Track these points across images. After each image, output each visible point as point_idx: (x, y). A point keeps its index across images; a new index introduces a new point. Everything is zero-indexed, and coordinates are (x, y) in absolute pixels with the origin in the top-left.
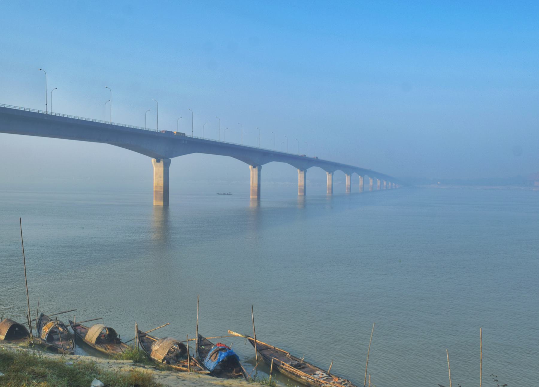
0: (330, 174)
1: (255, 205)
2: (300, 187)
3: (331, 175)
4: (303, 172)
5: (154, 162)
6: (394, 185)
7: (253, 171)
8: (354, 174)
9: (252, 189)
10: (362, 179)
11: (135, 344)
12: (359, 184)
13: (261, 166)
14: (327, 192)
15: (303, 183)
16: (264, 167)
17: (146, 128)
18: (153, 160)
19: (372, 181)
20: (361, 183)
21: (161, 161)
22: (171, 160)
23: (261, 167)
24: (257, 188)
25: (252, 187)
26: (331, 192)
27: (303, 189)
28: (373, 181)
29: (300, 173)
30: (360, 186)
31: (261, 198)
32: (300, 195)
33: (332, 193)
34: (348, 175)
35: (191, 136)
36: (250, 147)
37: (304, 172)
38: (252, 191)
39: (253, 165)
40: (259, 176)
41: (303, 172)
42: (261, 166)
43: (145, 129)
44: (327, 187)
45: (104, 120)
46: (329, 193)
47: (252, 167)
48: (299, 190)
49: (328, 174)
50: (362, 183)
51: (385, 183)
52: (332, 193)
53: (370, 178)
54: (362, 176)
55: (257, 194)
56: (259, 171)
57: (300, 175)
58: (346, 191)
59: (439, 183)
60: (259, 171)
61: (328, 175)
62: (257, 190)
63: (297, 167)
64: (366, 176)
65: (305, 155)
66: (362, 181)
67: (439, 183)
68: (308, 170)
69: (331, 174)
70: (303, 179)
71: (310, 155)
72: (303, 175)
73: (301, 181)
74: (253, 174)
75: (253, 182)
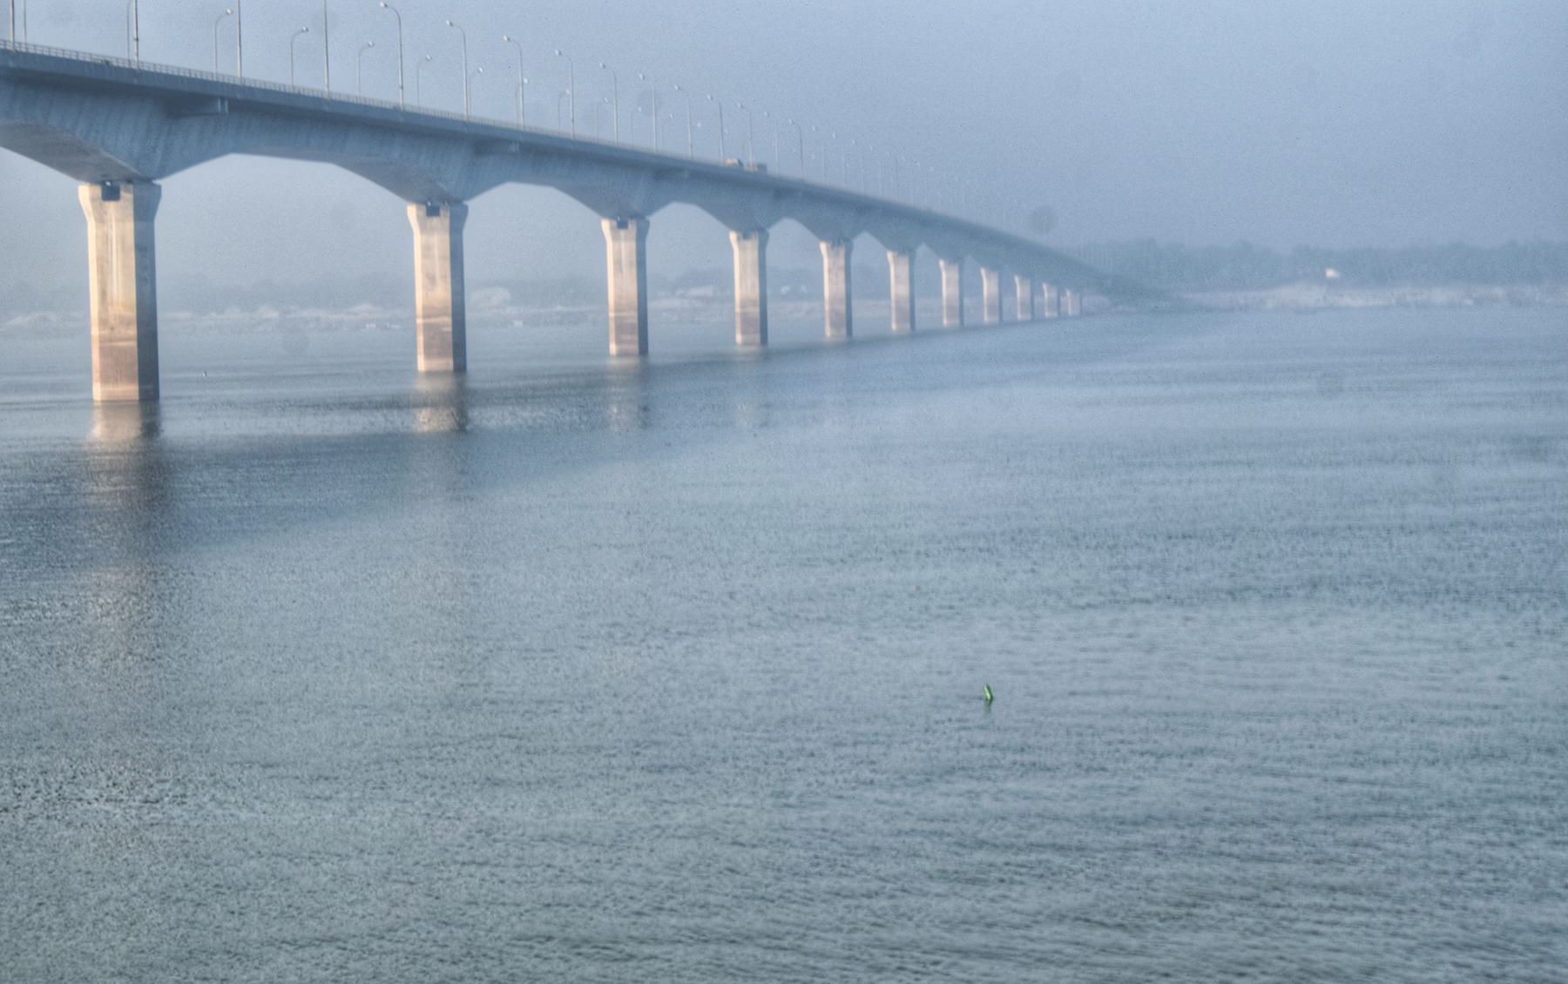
0: (622, 233)
1: (128, 430)
2: (425, 317)
3: (752, 245)
4: (441, 223)
5: (93, 200)
6: (1048, 293)
7: (101, 219)
8: (788, 232)
9: (102, 340)
10: (842, 262)
11: (173, 923)
12: (982, 292)
13: (158, 182)
14: (613, 348)
15: (443, 292)
16: (479, 207)
17: (129, 61)
18: (85, 193)
19: (904, 270)
20: (831, 285)
21: (123, 194)
22: (159, 187)
23: (465, 210)
24: (133, 331)
25: (103, 322)
26: (635, 348)
27: (449, 329)
28: (961, 280)
29: (423, 228)
30: (944, 303)
31: (163, 392)
32: (430, 374)
33: (764, 340)
34: (744, 235)
35: (462, 116)
36: (430, 113)
37: (447, 221)
38: (104, 352)
39: (103, 184)
40: (144, 249)
41: (441, 223)
42: (158, 182)
43: (127, 66)
44: (612, 314)
45: (126, 57)
46: (621, 354)
47: (98, 190)
48: (421, 339)
49: (612, 228)
50: (842, 287)
51: (988, 286)
52: (764, 340)
53: (890, 255)
54: (841, 241)
55: (136, 368)
56: (145, 213)
57: (615, 247)
58: (613, 348)
59: (1330, 273)
60: (145, 213)
61: (615, 238)
62: (134, 344)
63: (600, 205)
64: (865, 243)
65: (762, 167)
66: (842, 276)
67: (1330, 273)
68: (474, 205)
69: (632, 227)
70: (442, 267)
71: (783, 166)
72: (440, 241)
73: (430, 278)
74: (105, 241)
75: (103, 294)
